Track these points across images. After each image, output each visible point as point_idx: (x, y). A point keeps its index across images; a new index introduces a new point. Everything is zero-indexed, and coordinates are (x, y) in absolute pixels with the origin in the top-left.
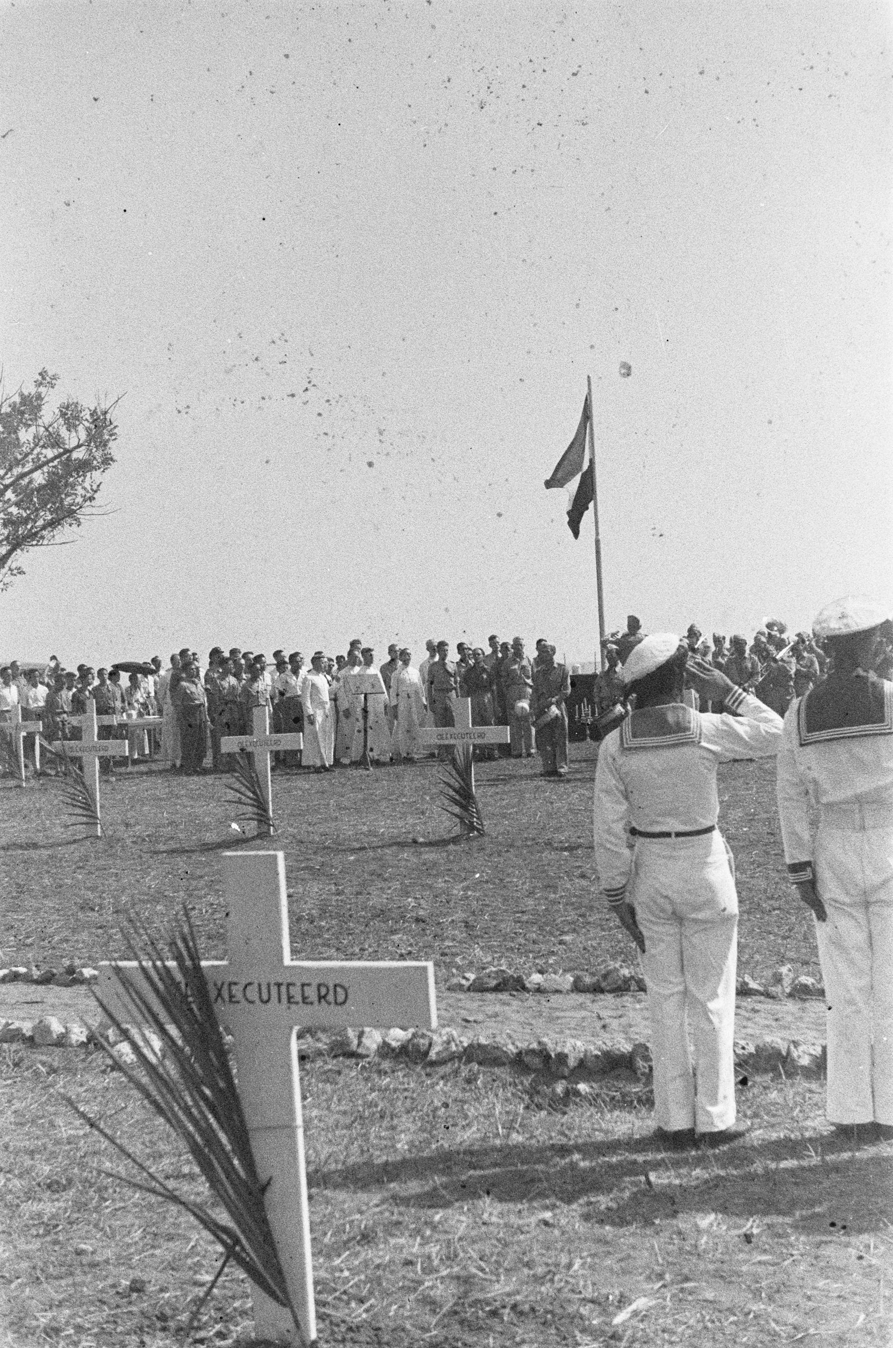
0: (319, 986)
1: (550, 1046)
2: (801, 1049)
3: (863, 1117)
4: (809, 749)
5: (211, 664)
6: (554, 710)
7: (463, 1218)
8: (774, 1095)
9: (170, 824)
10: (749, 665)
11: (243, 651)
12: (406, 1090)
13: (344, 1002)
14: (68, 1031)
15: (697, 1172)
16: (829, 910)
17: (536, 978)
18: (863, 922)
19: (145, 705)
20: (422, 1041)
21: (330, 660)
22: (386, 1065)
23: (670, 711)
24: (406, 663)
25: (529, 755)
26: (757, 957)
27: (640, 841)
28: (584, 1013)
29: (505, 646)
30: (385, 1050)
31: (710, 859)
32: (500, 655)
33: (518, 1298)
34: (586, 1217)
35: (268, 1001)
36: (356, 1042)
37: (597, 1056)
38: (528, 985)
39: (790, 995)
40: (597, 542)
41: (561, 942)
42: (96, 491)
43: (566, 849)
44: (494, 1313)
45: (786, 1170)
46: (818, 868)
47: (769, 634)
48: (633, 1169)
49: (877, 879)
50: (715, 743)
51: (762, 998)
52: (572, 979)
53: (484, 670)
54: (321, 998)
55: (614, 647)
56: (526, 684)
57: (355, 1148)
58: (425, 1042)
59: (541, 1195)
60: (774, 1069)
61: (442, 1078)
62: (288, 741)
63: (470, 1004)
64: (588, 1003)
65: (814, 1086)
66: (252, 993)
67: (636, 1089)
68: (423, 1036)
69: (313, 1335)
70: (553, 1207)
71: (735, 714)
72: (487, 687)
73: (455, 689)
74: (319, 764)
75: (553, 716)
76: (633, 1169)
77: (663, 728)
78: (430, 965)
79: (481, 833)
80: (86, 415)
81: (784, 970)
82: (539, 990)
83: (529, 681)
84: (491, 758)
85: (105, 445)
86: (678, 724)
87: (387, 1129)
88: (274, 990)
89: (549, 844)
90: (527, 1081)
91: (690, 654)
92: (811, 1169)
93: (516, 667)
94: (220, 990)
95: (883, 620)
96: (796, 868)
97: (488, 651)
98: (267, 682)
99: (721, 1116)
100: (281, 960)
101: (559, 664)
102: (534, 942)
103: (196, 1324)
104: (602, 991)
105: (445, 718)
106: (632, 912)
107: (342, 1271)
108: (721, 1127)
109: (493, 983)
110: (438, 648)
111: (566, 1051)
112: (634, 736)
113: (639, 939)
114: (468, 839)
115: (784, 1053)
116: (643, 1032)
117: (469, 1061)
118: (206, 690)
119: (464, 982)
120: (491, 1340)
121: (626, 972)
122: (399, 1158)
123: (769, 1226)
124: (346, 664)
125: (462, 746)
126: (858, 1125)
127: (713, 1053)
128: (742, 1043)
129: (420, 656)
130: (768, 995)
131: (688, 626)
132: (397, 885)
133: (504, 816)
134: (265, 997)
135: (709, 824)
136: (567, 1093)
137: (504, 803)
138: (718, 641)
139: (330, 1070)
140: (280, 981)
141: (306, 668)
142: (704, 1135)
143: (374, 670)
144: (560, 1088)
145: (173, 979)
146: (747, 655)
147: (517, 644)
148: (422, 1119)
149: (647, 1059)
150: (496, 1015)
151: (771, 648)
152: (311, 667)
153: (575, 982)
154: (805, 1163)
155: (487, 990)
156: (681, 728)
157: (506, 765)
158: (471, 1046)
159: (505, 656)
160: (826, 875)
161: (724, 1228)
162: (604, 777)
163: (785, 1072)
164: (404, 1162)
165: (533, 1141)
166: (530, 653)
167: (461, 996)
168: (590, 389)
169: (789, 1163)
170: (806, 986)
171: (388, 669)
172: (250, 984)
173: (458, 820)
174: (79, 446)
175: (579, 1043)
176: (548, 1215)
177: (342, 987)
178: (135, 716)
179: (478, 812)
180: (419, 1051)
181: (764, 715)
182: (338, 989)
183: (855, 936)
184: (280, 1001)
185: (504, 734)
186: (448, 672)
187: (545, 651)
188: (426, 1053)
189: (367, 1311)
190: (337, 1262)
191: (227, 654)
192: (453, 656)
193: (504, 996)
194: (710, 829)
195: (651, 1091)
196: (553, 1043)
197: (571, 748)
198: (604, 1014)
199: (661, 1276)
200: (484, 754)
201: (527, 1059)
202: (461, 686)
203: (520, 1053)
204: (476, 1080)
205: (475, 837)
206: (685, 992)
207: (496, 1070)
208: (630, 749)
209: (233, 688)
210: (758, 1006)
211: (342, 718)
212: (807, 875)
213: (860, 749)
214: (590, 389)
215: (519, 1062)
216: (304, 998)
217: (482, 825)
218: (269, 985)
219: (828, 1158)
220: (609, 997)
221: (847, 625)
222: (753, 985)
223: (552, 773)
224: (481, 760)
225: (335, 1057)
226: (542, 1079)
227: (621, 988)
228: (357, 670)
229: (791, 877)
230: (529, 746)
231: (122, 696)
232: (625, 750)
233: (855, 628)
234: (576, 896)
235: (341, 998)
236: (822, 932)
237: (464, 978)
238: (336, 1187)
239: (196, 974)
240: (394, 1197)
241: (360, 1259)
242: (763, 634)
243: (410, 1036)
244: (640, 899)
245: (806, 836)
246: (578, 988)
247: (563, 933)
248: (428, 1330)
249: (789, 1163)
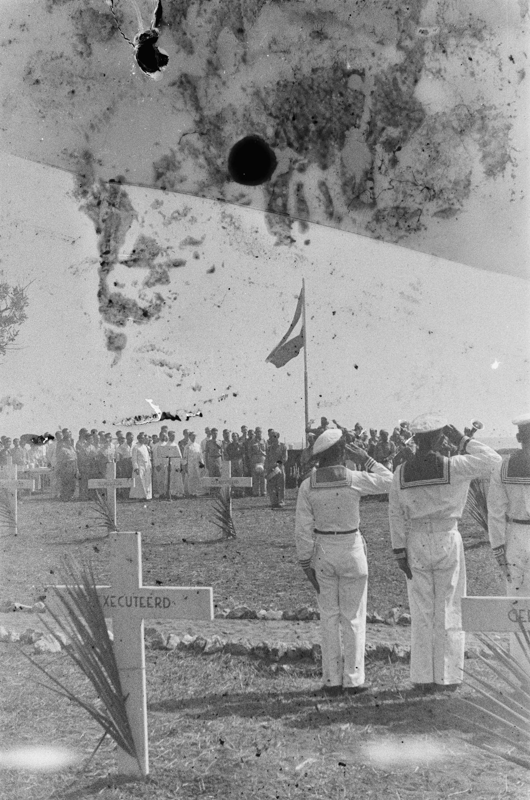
0: (156, 598)
1: (269, 645)
2: (399, 648)
3: (427, 679)
4: (405, 490)
5: (80, 438)
6: (278, 469)
7: (222, 724)
8: (385, 671)
9: (56, 529)
10: (389, 447)
11: (99, 431)
12: (192, 666)
14: (10, 634)
15: (341, 705)
16: (413, 573)
17: (263, 612)
18: (430, 579)
19: (40, 461)
20: (201, 642)
21: (150, 437)
22: (182, 654)
23: (336, 469)
24: (193, 441)
25: (263, 495)
26: (382, 604)
27: (319, 536)
28: (288, 631)
29: (250, 432)
30: (182, 647)
31: (354, 546)
32: (247, 437)
33: (249, 758)
34: (285, 725)
35: (130, 606)
36: (166, 642)
37: (294, 651)
38: (258, 616)
39: (398, 623)
40: (306, 373)
41: (277, 596)
42: (16, 335)
43: (282, 547)
44: (237, 765)
45: (387, 705)
46: (409, 552)
47: (402, 430)
48: (309, 704)
49: (438, 558)
50: (358, 486)
51: (383, 625)
52: (282, 613)
53: (239, 446)
54: (157, 604)
55: (313, 434)
56: (263, 455)
57: (166, 693)
58: (204, 642)
59: (263, 714)
60: (386, 658)
61: (212, 661)
62: (124, 483)
63: (227, 625)
64: (291, 625)
65: (405, 667)
66: (123, 601)
67: (313, 668)
68: (202, 639)
69: (147, 772)
70: (268, 720)
71: (369, 471)
72: (239, 456)
73: (221, 456)
74: (141, 497)
75: (277, 473)
76: (309, 704)
77: (332, 478)
78: (211, 589)
79: (234, 537)
80: (11, 290)
81: (395, 610)
82: (264, 618)
83: (264, 453)
84: (241, 496)
85: (22, 309)
86: (340, 475)
87: (183, 685)
88: (134, 600)
89: (272, 544)
90: (256, 663)
91: (356, 439)
92: (399, 705)
93: (257, 444)
94: (106, 600)
95: (444, 425)
96: (397, 551)
97: (241, 435)
98: (112, 448)
99: (356, 679)
100: (138, 586)
101: (282, 444)
102: (263, 595)
103: (87, 770)
104: (298, 619)
105: (215, 473)
106: (314, 572)
107: (160, 748)
108: (355, 685)
109: (240, 614)
110: (212, 432)
111: (278, 647)
112: (317, 482)
113: (317, 587)
115: (391, 650)
116: (318, 640)
117: (226, 653)
118: (77, 452)
119: (224, 613)
120: (235, 776)
121: (311, 609)
122: (189, 698)
123: (376, 729)
124: (158, 440)
125: (225, 487)
126: (425, 684)
127: (352, 647)
128: (370, 644)
129: (201, 437)
130: (386, 623)
131: (355, 424)
132: (186, 564)
134: (129, 603)
135: (355, 528)
136: (277, 669)
138: (373, 433)
139: (152, 656)
141: (135, 442)
142: (346, 688)
143: (175, 444)
144: (274, 667)
145: (83, 595)
146: (388, 441)
147: (258, 431)
148: (200, 680)
149: (320, 652)
150: (241, 631)
151: (402, 438)
152: (137, 441)
153: (284, 615)
154: (397, 702)
155: (236, 618)
156: (342, 478)
157: (249, 501)
158: (227, 645)
159: (251, 438)
160: (412, 555)
161: (354, 730)
162: (301, 503)
163: (391, 660)
164: (192, 699)
165: (259, 691)
166: (265, 437)
167: (222, 621)
168: (304, 286)
169: (390, 702)
170: (407, 619)
171: (182, 444)
173: (221, 530)
174: (6, 309)
175: (284, 644)
176: (265, 723)
177: (168, 600)
178: (33, 467)
180: (199, 647)
181: (384, 472)
183: (427, 587)
184: (136, 606)
185: (248, 482)
186: (218, 446)
187: (273, 436)
188: (203, 648)
189: (173, 764)
190: (158, 743)
191: (89, 432)
192: (220, 438)
193: (245, 621)
194: (355, 530)
195: (321, 669)
196: (271, 644)
197: (286, 492)
198: (299, 631)
199: (320, 750)
200: (238, 493)
201: (256, 652)
202: (225, 455)
203: (253, 649)
204: (230, 661)
206: (340, 615)
207: (241, 658)
208: (315, 488)
209: (92, 452)
210: (380, 629)
211: (156, 471)
212: (402, 555)
213: (431, 492)
214: (304, 286)
215: (253, 653)
216: (148, 604)
217: (235, 532)
220: (302, 623)
221: (425, 428)
222: (379, 618)
223: (275, 506)
224: (235, 498)
225: (155, 649)
226: (264, 662)
227: (309, 618)
228: (165, 443)
229: (395, 556)
230: (262, 490)
231: (27, 455)
232: (311, 488)
233: (429, 429)
234: (286, 572)
235: (167, 605)
236: (410, 583)
237: (224, 611)
238: (157, 710)
239: (93, 594)
240: (187, 715)
241: (170, 742)
242: (398, 430)
243: (195, 639)
244: (317, 566)
245: (403, 535)
246: (285, 618)
247: (278, 591)
248: (204, 772)
249: (390, 702)
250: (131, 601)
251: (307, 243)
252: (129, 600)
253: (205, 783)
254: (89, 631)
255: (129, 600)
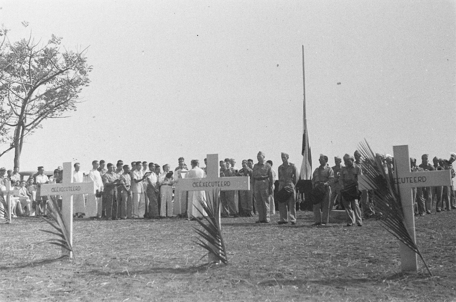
0: (225, 182)
13: (425, 181)
88: (215, 183)
114: (214, 267)
133: (249, 247)
134: (403, 181)
137: (252, 239)
140: (217, 181)
172: (210, 182)
179: (223, 246)
182: (424, 178)
184: (216, 186)
205: (221, 266)
218: (404, 178)
219: (29, 204)
250: (405, 180)
251: (25, 24)
252: (403, 180)
253: (105, 266)
254: (219, 196)
255: (403, 180)
